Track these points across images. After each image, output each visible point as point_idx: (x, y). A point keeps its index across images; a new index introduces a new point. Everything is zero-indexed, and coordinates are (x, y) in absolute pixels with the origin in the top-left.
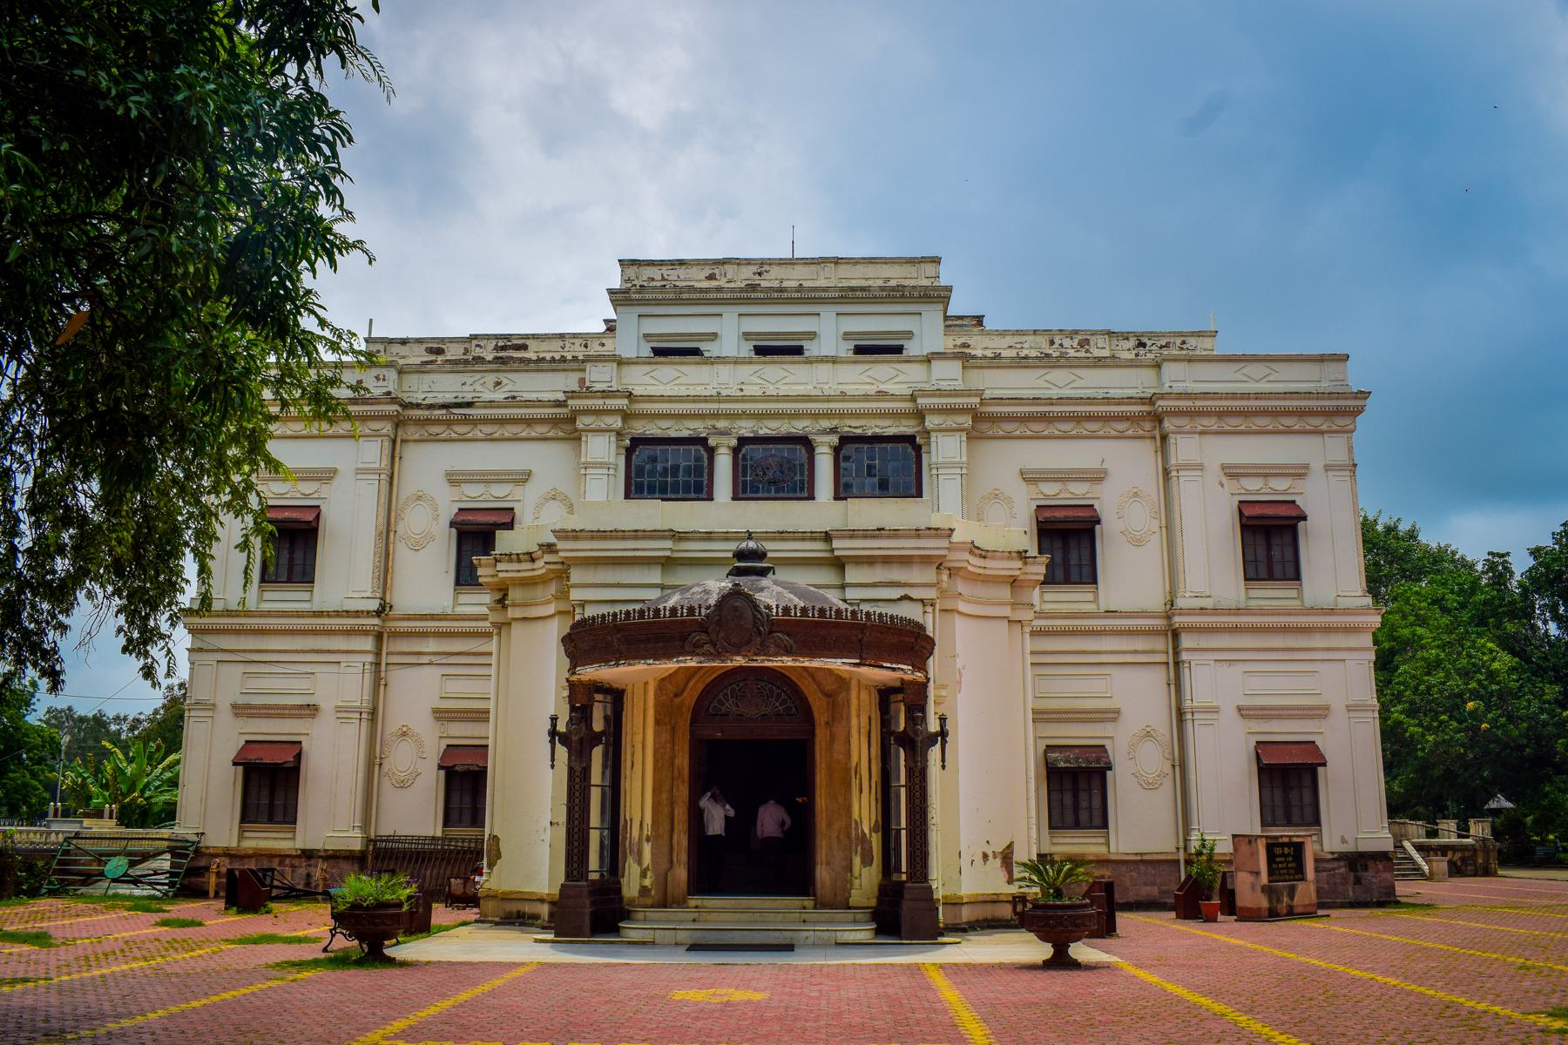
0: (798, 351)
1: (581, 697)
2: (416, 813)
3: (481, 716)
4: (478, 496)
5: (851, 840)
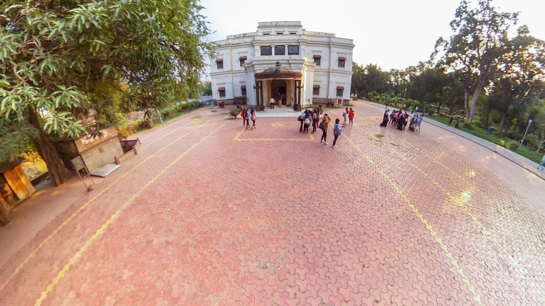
0: (282, 34)
1: (257, 83)
2: (239, 94)
3: (245, 82)
4: (243, 55)
5: (291, 99)
